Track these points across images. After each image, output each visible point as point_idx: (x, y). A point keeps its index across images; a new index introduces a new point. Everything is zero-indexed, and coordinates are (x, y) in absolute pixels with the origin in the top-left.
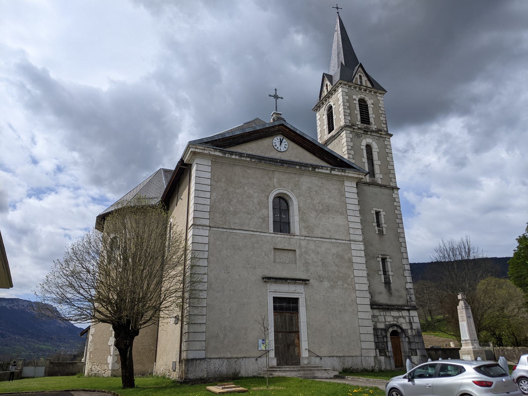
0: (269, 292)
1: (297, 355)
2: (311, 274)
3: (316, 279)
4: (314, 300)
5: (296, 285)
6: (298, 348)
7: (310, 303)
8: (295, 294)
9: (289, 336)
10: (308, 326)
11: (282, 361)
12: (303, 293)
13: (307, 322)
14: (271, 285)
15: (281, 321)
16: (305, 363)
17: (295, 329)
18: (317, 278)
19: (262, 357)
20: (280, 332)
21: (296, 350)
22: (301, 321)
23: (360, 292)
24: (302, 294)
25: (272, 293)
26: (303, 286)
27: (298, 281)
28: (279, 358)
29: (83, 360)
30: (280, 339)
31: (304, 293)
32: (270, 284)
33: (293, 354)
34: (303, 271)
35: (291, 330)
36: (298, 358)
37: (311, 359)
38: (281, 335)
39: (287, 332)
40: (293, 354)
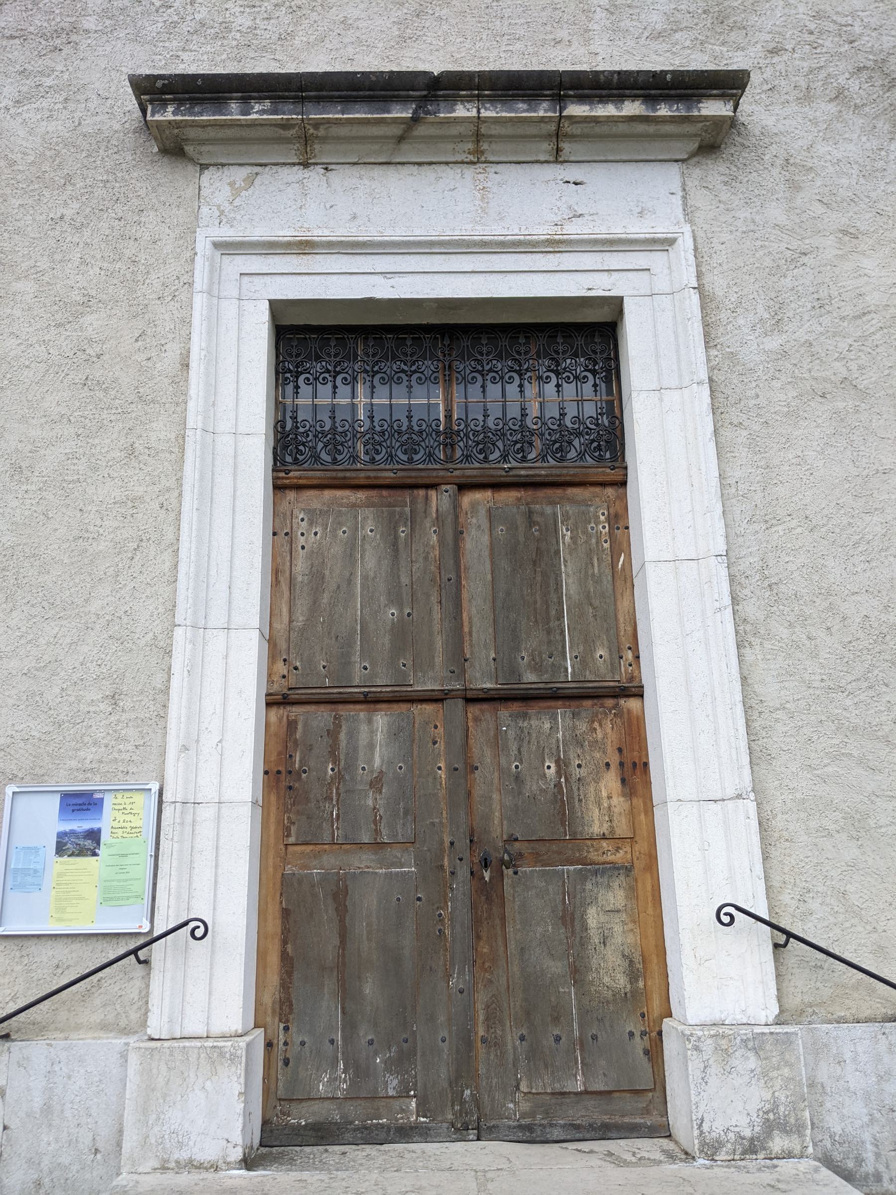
0: (226, 247)
1: (622, 981)
2: (774, 52)
3: (840, 95)
4: (821, 305)
5: (573, 172)
6: (632, 891)
7: (773, 343)
8: (568, 261)
9: (497, 742)
10: (750, 609)
11: (392, 1065)
12: (665, 243)
13: (730, 557)
14: (250, 181)
15: (394, 573)
16: (716, 1127)
17: (583, 661)
18: (854, 85)
19: (40, 1030)
20: (371, 701)
21: (593, 918)
22: (650, 553)
23: (309, 1093)
24: (655, 260)
25: (255, 264)
26: (674, 170)
27: (582, 99)
28: (350, 1026)
29: (527, 678)
30: (376, 784)
31: (685, 243)
32: (240, 174)
33: (556, 967)
34: (658, 36)
35: (530, 677)
36: (633, 1025)
37: (817, 1050)
38: (394, 734)
39: (471, 699)
40: (556, 967)
